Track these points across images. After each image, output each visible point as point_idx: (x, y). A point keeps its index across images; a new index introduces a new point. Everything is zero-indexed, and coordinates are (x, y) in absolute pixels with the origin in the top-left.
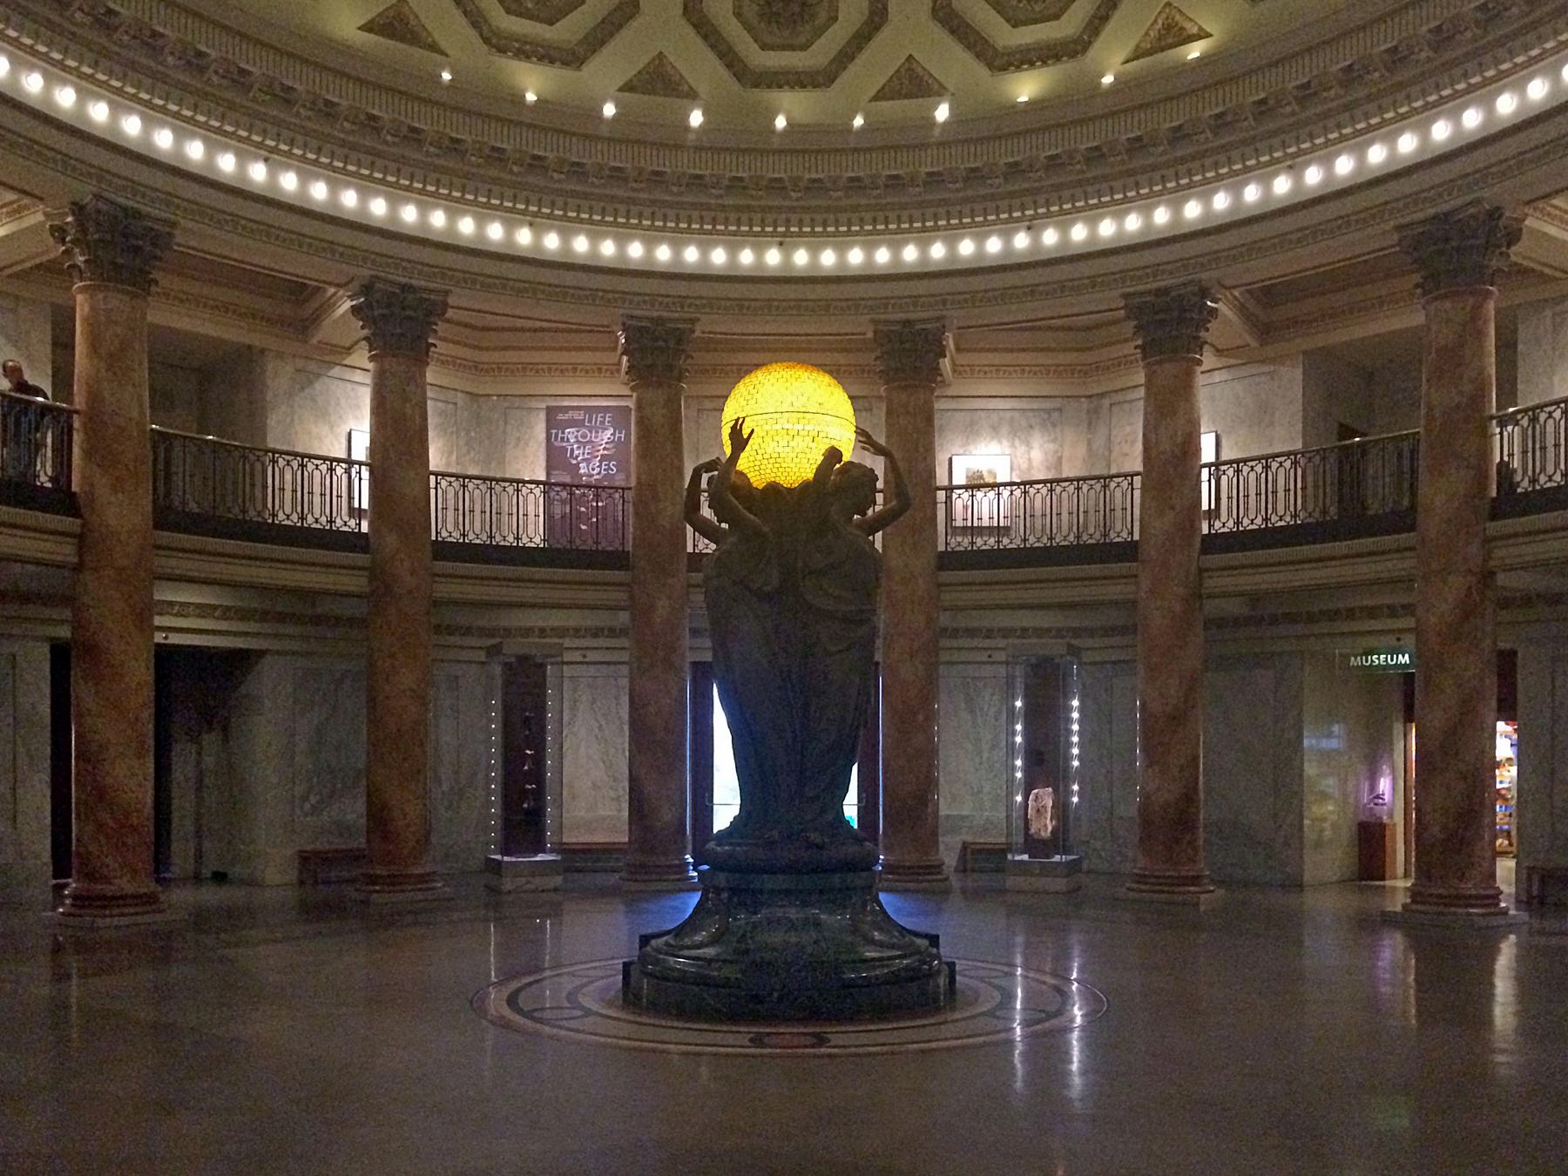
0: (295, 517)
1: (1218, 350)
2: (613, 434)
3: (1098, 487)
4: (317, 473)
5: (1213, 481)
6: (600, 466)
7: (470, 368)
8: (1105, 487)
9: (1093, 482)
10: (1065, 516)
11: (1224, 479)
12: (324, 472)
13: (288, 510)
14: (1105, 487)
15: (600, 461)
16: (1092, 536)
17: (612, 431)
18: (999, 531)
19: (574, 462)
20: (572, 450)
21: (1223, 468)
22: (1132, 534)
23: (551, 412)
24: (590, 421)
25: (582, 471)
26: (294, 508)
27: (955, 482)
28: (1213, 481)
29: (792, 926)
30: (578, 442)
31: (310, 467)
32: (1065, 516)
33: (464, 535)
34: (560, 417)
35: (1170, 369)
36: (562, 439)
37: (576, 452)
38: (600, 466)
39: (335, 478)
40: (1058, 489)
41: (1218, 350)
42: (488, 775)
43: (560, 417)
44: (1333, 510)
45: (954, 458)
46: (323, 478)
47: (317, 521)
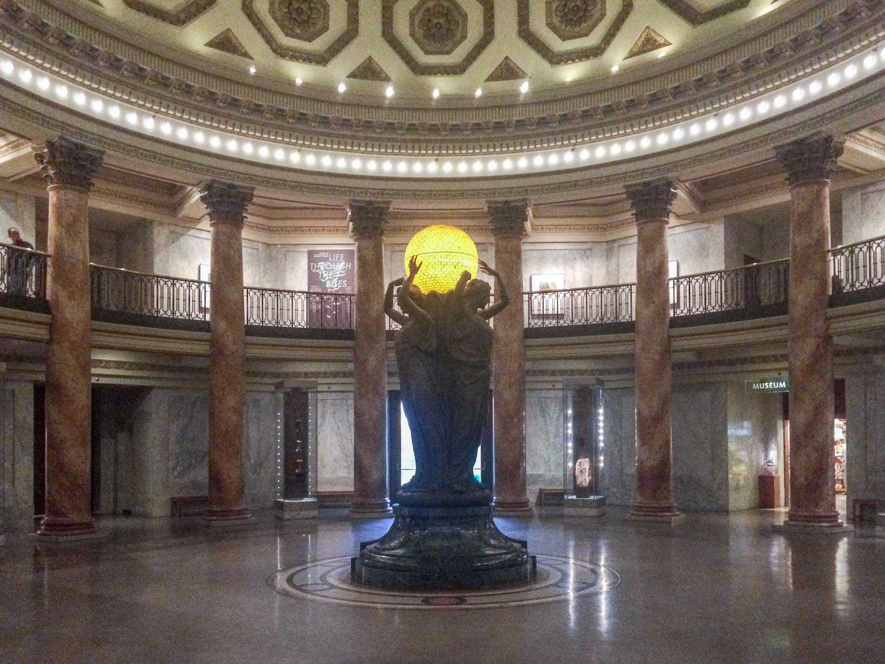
0: (169, 313)
2: (345, 265)
5: (676, 288)
6: (337, 283)
7: (266, 230)
10: (594, 308)
11: (682, 287)
12: (185, 288)
15: (338, 280)
16: (609, 318)
17: (344, 263)
18: (559, 316)
19: (323, 281)
20: (322, 274)
21: (681, 280)
22: (631, 317)
23: (311, 254)
24: (332, 258)
25: (327, 286)
28: (676, 288)
29: (445, 537)
30: (325, 270)
36: (317, 268)
37: (324, 276)
38: (337, 283)
43: (316, 256)
44: (742, 303)
45: (533, 277)
47: (181, 315)
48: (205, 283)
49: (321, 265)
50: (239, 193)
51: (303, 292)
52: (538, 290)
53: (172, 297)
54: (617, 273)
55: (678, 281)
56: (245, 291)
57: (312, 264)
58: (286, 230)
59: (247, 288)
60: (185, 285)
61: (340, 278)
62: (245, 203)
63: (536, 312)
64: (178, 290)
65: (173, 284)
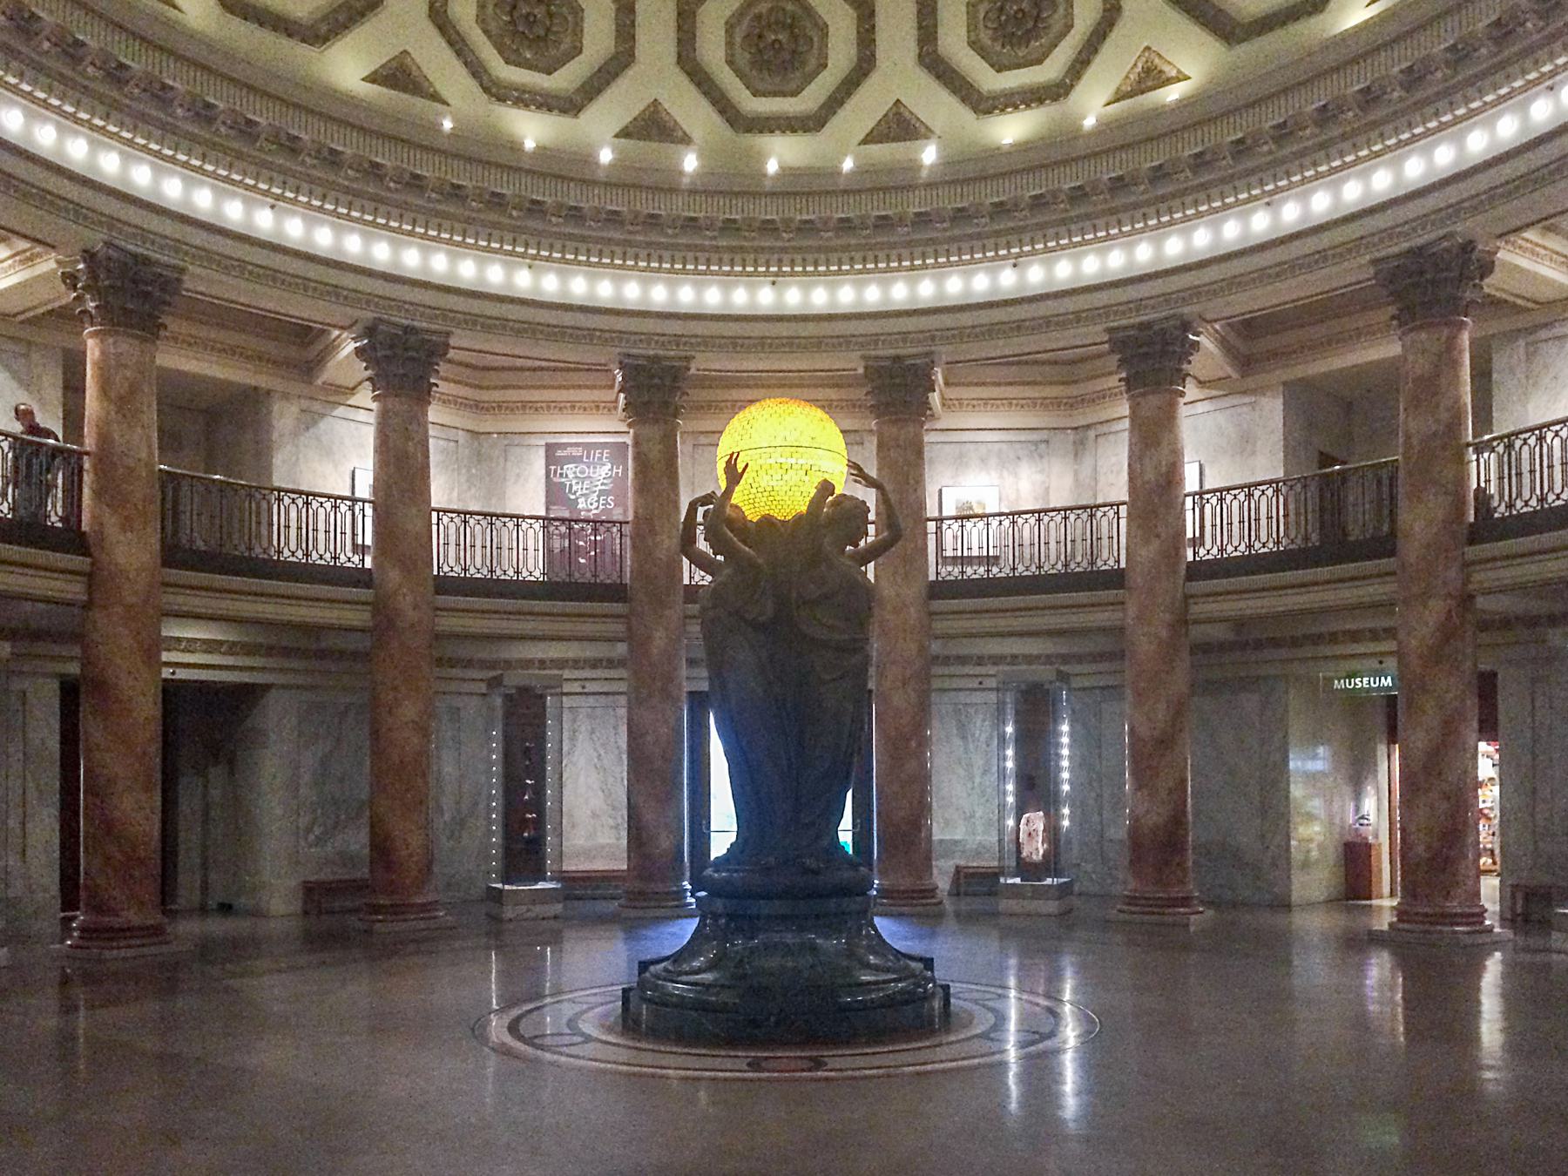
1: (1200, 382)
2: (611, 470)
3: (1085, 516)
4: (321, 510)
5: (1197, 510)
6: (598, 501)
7: (471, 407)
8: (1092, 516)
9: (1080, 512)
10: (1053, 545)
13: (293, 547)
14: (1092, 516)
15: (599, 496)
16: (1080, 564)
17: (609, 466)
18: (990, 560)
19: (573, 497)
20: (571, 486)
21: (1206, 496)
22: (1118, 562)
23: (550, 449)
24: (588, 457)
25: (580, 506)
26: (299, 545)
27: (945, 514)
28: (1197, 510)
30: (576, 477)
31: (315, 505)
32: (1053, 545)
33: (1039, 520)
34: (559, 453)
35: (1154, 400)
36: (561, 475)
37: (574, 488)
38: (598, 501)
39: (339, 515)
40: (1046, 519)
41: (1200, 382)
42: (489, 805)
43: (559, 453)
44: (1315, 537)
45: (944, 490)
46: (327, 516)
47: (321, 558)
48: (364, 501)
49: (569, 469)
50: (424, 341)
51: (537, 518)
52: (953, 513)
53: (304, 526)
54: (1093, 484)
55: (1201, 498)
56: (434, 514)
57: (553, 468)
58: (507, 408)
59: (438, 511)
60: (328, 505)
61: (602, 493)
62: (435, 360)
63: (949, 553)
64: (316, 514)
65: (307, 503)
